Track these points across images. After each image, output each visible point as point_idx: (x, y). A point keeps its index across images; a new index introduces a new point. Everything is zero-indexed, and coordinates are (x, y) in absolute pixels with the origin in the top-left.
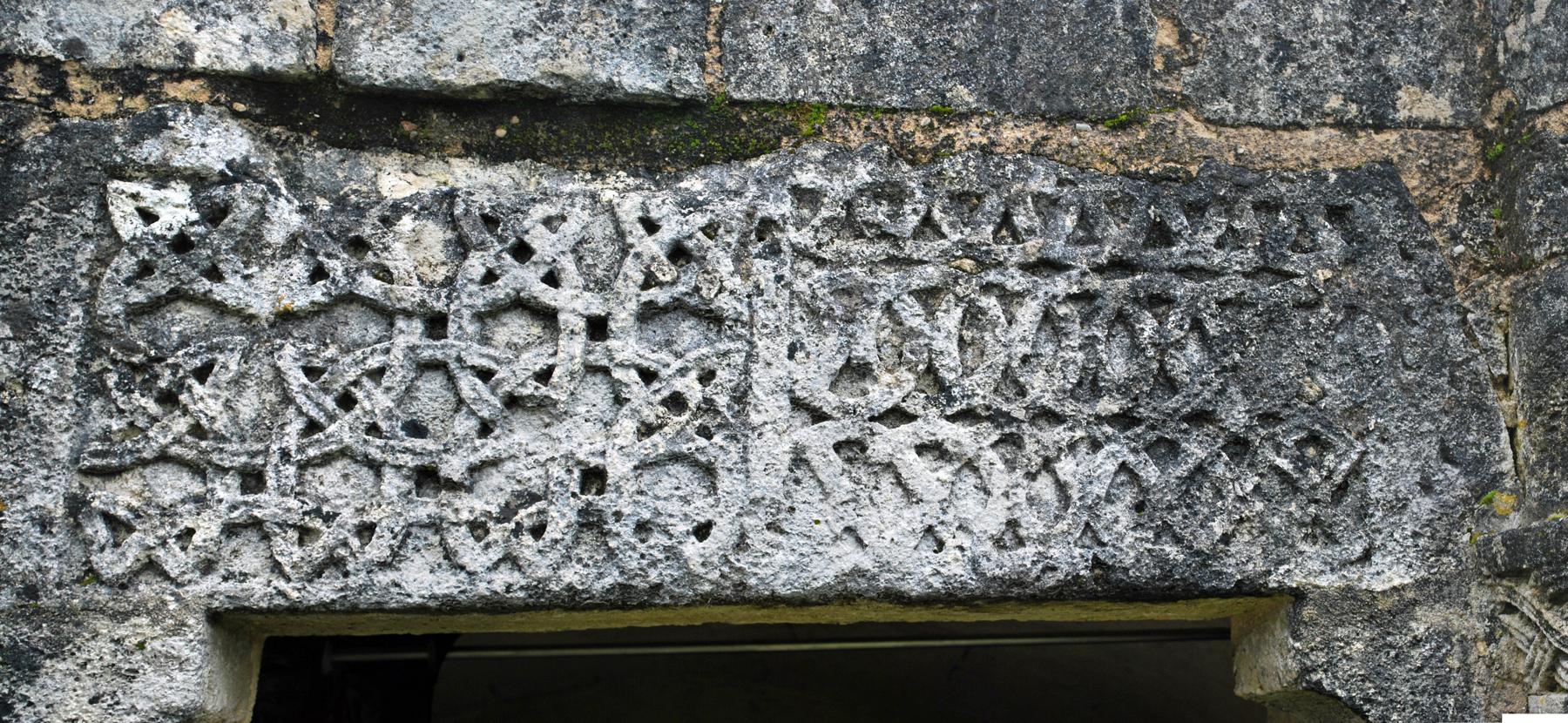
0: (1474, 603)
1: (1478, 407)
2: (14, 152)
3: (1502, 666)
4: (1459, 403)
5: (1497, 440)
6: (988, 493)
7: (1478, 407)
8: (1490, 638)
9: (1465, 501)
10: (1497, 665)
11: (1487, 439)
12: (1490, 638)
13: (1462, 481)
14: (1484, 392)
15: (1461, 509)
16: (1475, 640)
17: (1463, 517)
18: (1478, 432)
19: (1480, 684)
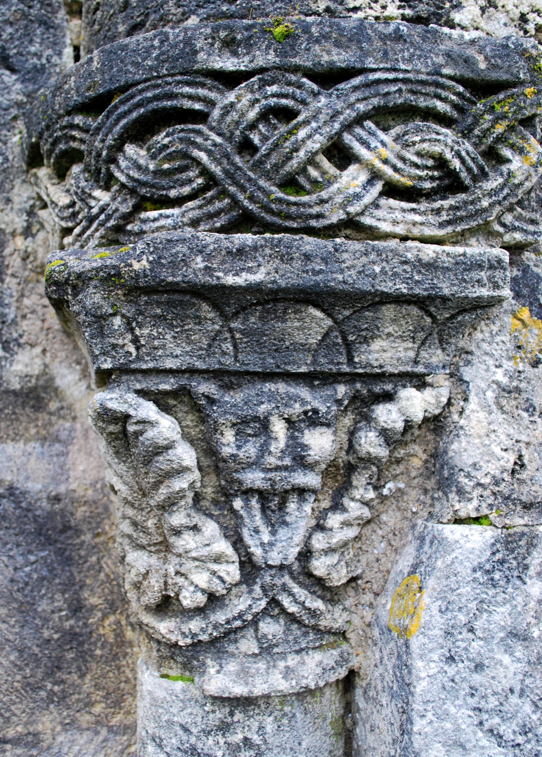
0: (16, 199)
1: (45, 23)
2: (2, 334)
3: (36, 259)
4: (25, 16)
5: (60, 54)
6: (424, 716)
7: (45, 23)
8: (27, 232)
9: (19, 105)
10: (31, 258)
11: (49, 52)
12: (27, 232)
13: (18, 86)
14: (54, 12)
15: (14, 112)
16: (13, 234)
17: (15, 118)
18: (41, 44)
19: (13, 275)
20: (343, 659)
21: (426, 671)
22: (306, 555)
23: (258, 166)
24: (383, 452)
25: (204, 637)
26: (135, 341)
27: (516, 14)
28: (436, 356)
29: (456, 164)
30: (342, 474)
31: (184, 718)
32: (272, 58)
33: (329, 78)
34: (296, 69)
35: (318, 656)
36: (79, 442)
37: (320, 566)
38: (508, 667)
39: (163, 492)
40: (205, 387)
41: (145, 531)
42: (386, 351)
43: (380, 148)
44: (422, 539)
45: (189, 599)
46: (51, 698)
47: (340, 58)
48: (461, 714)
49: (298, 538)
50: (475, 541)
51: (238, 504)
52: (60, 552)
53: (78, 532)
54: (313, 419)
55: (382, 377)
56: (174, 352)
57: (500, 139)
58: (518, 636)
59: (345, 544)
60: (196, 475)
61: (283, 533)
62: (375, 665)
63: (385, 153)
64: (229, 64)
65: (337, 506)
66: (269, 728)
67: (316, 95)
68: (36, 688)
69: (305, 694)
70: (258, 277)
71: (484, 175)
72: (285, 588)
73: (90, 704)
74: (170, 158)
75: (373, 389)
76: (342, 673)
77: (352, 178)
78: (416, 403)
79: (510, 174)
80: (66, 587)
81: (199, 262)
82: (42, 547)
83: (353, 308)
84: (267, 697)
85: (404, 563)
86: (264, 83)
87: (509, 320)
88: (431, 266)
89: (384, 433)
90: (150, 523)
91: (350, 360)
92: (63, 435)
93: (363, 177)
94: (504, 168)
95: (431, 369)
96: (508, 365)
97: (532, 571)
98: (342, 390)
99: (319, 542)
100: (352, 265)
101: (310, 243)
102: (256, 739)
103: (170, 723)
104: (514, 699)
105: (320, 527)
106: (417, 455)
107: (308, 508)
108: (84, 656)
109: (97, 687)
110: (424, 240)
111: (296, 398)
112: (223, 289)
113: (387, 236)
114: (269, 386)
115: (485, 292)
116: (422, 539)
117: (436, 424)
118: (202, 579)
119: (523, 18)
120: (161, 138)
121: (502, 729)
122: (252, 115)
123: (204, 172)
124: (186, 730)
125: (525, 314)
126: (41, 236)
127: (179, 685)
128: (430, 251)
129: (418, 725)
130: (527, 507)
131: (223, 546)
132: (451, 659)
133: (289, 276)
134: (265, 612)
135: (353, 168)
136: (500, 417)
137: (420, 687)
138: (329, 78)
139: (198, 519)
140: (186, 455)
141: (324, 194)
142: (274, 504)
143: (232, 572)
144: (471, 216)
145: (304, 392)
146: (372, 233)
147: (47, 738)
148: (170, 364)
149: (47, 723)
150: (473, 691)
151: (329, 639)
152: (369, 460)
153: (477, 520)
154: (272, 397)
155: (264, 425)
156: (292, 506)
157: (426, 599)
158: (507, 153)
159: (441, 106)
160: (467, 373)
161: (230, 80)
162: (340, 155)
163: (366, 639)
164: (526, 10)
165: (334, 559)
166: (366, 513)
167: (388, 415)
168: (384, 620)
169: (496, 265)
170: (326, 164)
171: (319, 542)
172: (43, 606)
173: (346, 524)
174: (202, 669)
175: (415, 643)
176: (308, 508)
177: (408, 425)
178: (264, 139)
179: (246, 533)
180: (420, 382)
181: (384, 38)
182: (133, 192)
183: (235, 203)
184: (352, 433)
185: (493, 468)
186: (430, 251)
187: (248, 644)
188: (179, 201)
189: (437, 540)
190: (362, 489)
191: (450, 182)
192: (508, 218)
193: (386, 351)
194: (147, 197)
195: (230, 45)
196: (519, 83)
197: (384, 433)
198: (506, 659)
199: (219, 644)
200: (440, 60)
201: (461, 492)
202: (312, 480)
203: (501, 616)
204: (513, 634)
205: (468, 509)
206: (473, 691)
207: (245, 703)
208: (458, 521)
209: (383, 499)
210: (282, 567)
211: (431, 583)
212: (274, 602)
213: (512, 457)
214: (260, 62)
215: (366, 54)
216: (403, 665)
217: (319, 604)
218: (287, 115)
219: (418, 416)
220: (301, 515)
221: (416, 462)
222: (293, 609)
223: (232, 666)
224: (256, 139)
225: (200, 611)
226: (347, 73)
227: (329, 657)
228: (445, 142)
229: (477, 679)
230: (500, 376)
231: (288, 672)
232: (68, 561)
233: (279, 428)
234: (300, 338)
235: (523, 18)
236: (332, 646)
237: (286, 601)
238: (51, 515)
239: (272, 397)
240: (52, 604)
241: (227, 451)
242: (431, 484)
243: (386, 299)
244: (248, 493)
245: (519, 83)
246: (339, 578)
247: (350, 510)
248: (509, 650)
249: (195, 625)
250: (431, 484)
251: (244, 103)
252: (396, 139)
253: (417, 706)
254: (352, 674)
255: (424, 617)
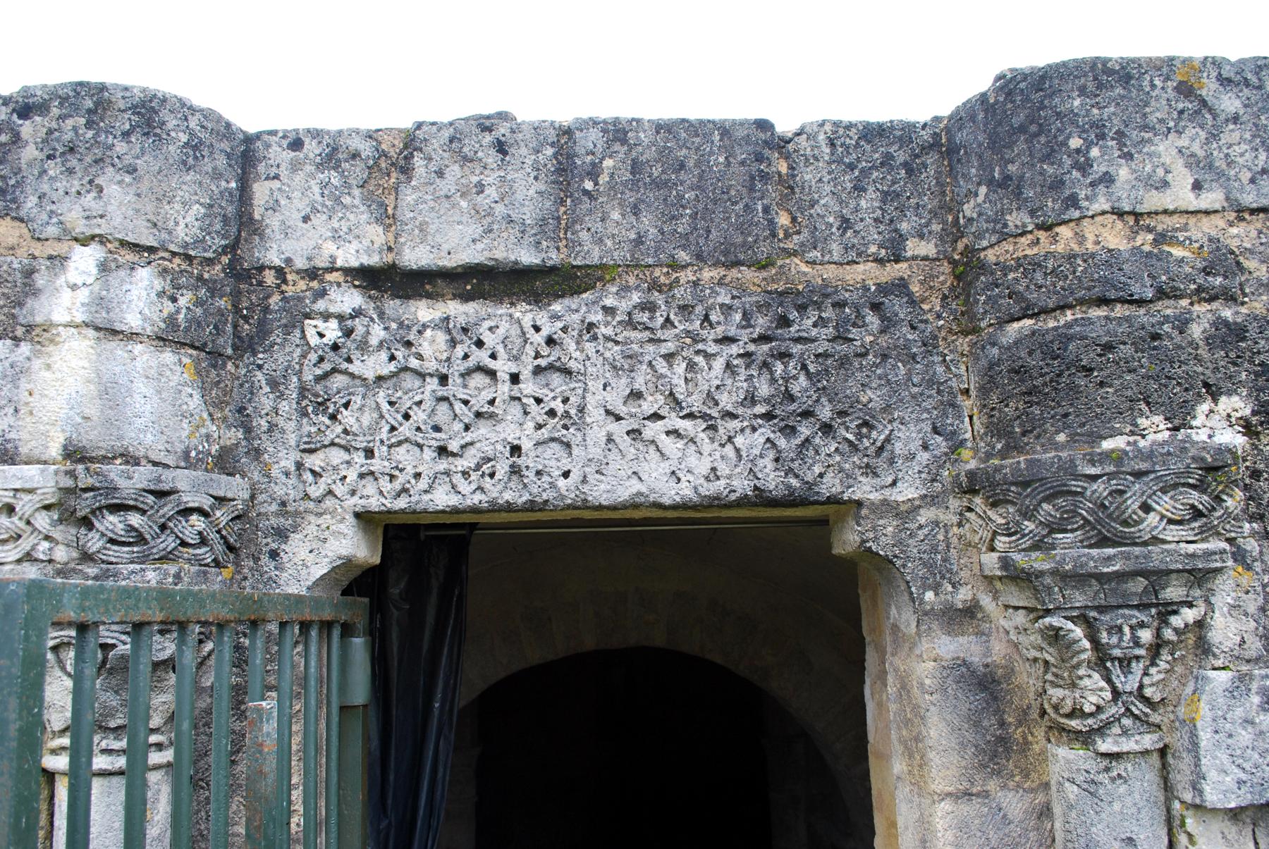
4: (942, 403)
5: (963, 422)
8: (960, 525)
9: (946, 454)
12: (960, 525)
15: (944, 458)
20: (1161, 739)
21: (1205, 737)
22: (1141, 687)
23: (1110, 516)
24: (1175, 638)
25: (1095, 727)
26: (1063, 596)
27: (1225, 414)
28: (1197, 592)
29: (1201, 507)
30: (1155, 650)
31: (1087, 767)
32: (1112, 468)
33: (1138, 475)
34: (1123, 473)
35: (1149, 736)
36: (994, 634)
37: (1148, 692)
38: (1245, 736)
39: (1075, 660)
40: (1093, 614)
41: (1063, 678)
42: (1173, 592)
43: (1165, 504)
44: (1197, 678)
45: (1088, 708)
46: (993, 772)
47: (1143, 466)
48: (1224, 757)
49: (1138, 679)
50: (1223, 677)
51: (1109, 664)
52: (991, 694)
53: (999, 683)
54: (1142, 625)
55: (1172, 603)
56: (1079, 599)
57: (1222, 492)
58: (1249, 722)
59: (1158, 682)
60: (1090, 653)
61: (1130, 677)
62: (1178, 740)
63: (1167, 506)
64: (1092, 471)
65: (1153, 664)
66: (1130, 769)
67: (1133, 483)
68: (986, 767)
69: (1146, 753)
70: (1117, 568)
71: (1214, 509)
72: (1132, 703)
73: (1013, 776)
74: (1066, 512)
75: (1168, 610)
76: (1161, 745)
77: (1152, 519)
78: (1189, 615)
79: (1227, 508)
80: (996, 712)
81: (1092, 564)
82: (982, 691)
83: (1157, 577)
84: (1128, 753)
85: (1189, 689)
86: (1109, 480)
87: (1232, 572)
88: (1193, 556)
89: (1175, 630)
90: (1065, 675)
91: (1157, 598)
92: (987, 631)
93: (1158, 518)
94: (1224, 505)
95: (1195, 598)
96: (1233, 594)
97: (1253, 691)
98: (1153, 611)
99: (1146, 680)
100: (1156, 557)
101: (1137, 550)
102: (1124, 774)
103: (1078, 770)
104: (1249, 751)
105: (1146, 674)
106: (1191, 639)
107: (1141, 665)
108: (1008, 750)
109: (1016, 766)
110: (1188, 542)
111: (1134, 616)
112: (1103, 574)
113: (1170, 542)
114: (1121, 611)
115: (1218, 565)
116: (1197, 678)
117: (1200, 624)
118: (1094, 699)
119: (1229, 416)
120: (1060, 501)
121: (1244, 765)
122: (1105, 494)
123: (1084, 518)
124: (1087, 772)
125: (1240, 569)
126: (967, 526)
127: (1081, 752)
128: (1191, 548)
129: (1203, 761)
130: (1248, 661)
131: (1103, 684)
132: (1216, 732)
133: (1130, 566)
134: (1123, 715)
135: (1152, 514)
136: (1231, 619)
137: (1203, 744)
138: (1138, 475)
139: (1090, 672)
140: (1086, 644)
141: (1141, 527)
142: (1125, 664)
143: (1108, 695)
144: (1209, 529)
145: (1136, 613)
146: (1164, 542)
147: (993, 793)
148: (1077, 605)
149: (992, 785)
150: (1228, 747)
151: (1153, 728)
152: (1169, 642)
153: (1223, 668)
154: (1123, 616)
155: (1120, 629)
156: (1134, 664)
157: (1202, 704)
158: (1225, 497)
159: (1191, 481)
160: (1213, 600)
161: (1094, 478)
162: (1146, 508)
163: (1172, 729)
164: (1229, 411)
165: (1154, 689)
166: (1168, 667)
167: (1176, 621)
168: (1181, 716)
169: (1223, 552)
170: (1140, 513)
171: (1146, 680)
172: (985, 723)
173: (1159, 672)
174: (1094, 742)
175: (1199, 724)
176: (1141, 665)
177: (1186, 625)
178: (1111, 503)
179: (1114, 677)
180: (1190, 605)
181: (1162, 455)
182: (1047, 526)
183: (1100, 532)
184: (1158, 629)
185: (1229, 644)
186: (1191, 548)
187: (1116, 730)
188: (1072, 531)
189: (1207, 678)
190: (1165, 655)
191: (1197, 514)
192: (1228, 527)
193: (1173, 592)
194: (1055, 527)
195: (1092, 462)
196: (1230, 465)
197: (1175, 630)
198: (1244, 733)
199: (1101, 731)
200: (1189, 461)
201: (1214, 655)
202: (1142, 652)
203: (1239, 712)
204: (1246, 721)
205: (1219, 663)
206: (1228, 747)
207: (1116, 756)
208: (1215, 669)
209: (1174, 659)
210: (1131, 693)
211: (1204, 697)
212: (1128, 709)
213: (1239, 638)
214: (1107, 470)
215: (1155, 463)
216: (1193, 735)
217: (1148, 710)
218: (1122, 492)
219: (1191, 621)
220: (1138, 668)
221: (1191, 642)
222: (1137, 712)
223: (1109, 740)
224: (1107, 503)
225: (1091, 715)
226: (1146, 473)
227: (1155, 737)
228: (1195, 497)
229: (1230, 741)
230: (1229, 600)
231: (1137, 742)
232: (996, 699)
233: (1126, 630)
234: (1134, 590)
235: (1229, 416)
236: (1155, 732)
237: (1134, 709)
238: (985, 675)
239: (1123, 616)
240: (989, 722)
241: (1104, 641)
242: (1198, 652)
243: (1172, 571)
244: (1113, 659)
245: (1230, 465)
246: (1157, 698)
247: (350, 519)
248: (1245, 729)
249: (1090, 721)
250: (1198, 652)
251: (1100, 488)
252: (1171, 498)
253: (1202, 753)
254: (1166, 746)
255: (1202, 712)
